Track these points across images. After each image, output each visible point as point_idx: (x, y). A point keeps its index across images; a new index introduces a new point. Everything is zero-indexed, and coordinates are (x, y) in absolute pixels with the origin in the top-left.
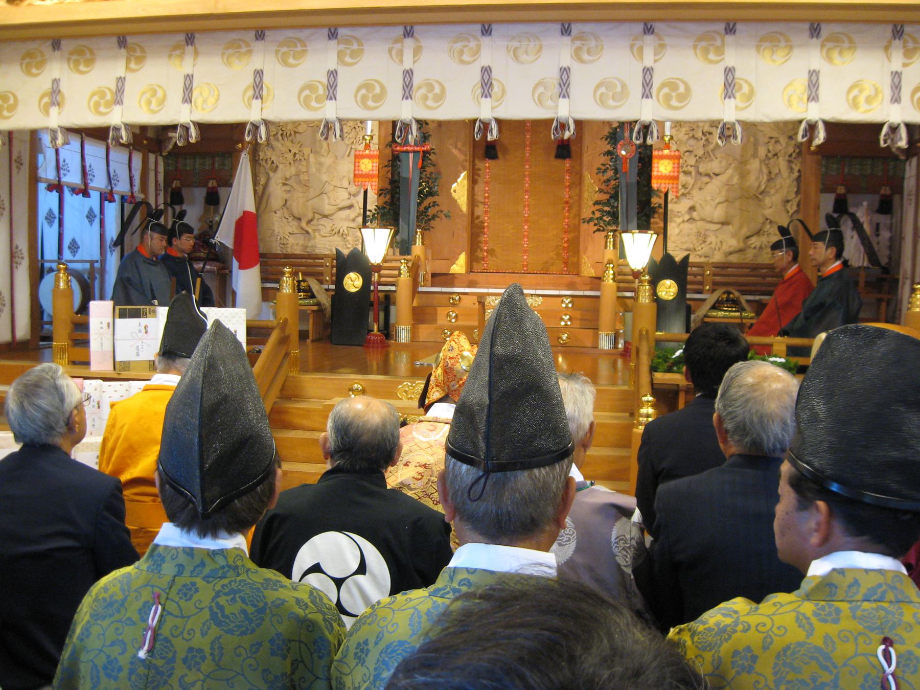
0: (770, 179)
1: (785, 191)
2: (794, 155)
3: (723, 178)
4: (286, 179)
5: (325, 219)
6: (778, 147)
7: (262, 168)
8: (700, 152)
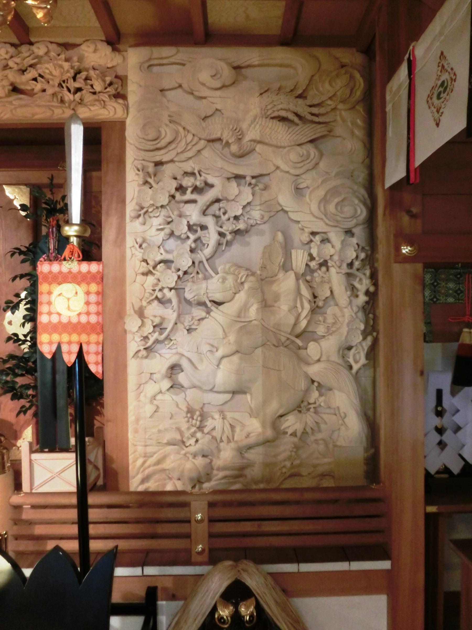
0: (315, 310)
1: (344, 330)
2: (357, 264)
3: (230, 309)
6: (328, 250)
8: (185, 262)
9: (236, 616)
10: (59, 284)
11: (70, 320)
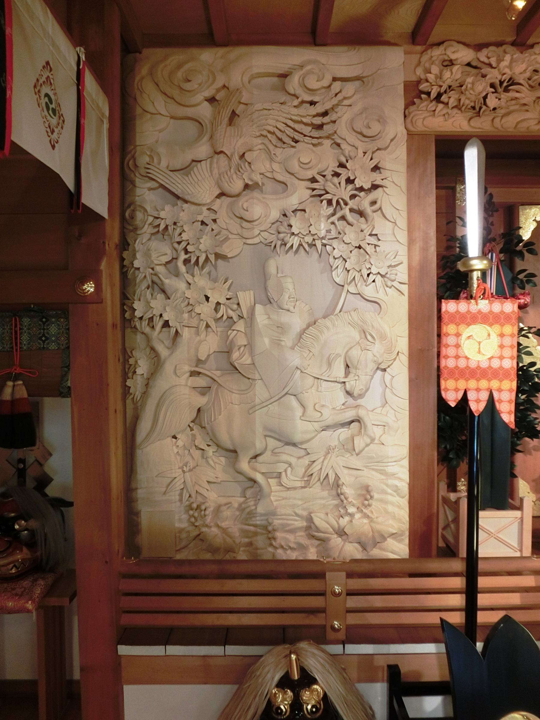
4: (199, 362)
5: (289, 449)
7: (139, 338)
9: (297, 704)
10: (469, 325)
11: (478, 364)
